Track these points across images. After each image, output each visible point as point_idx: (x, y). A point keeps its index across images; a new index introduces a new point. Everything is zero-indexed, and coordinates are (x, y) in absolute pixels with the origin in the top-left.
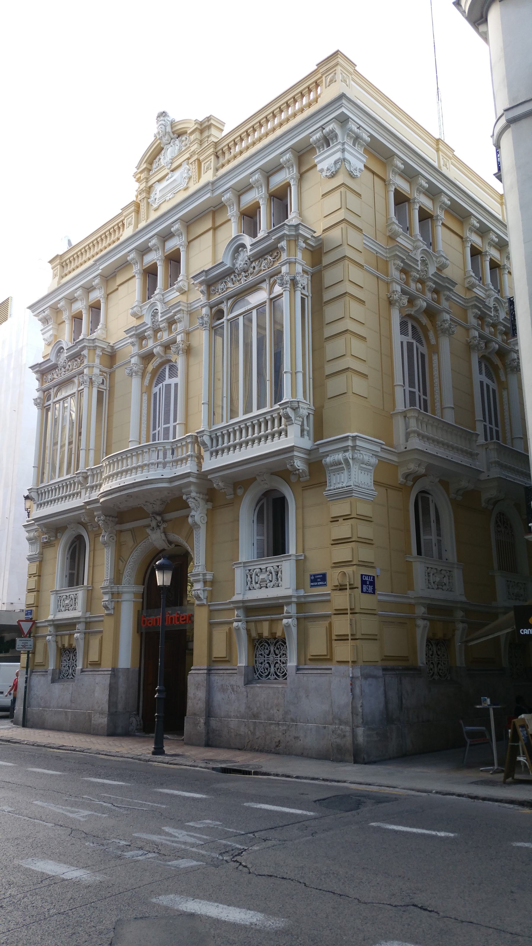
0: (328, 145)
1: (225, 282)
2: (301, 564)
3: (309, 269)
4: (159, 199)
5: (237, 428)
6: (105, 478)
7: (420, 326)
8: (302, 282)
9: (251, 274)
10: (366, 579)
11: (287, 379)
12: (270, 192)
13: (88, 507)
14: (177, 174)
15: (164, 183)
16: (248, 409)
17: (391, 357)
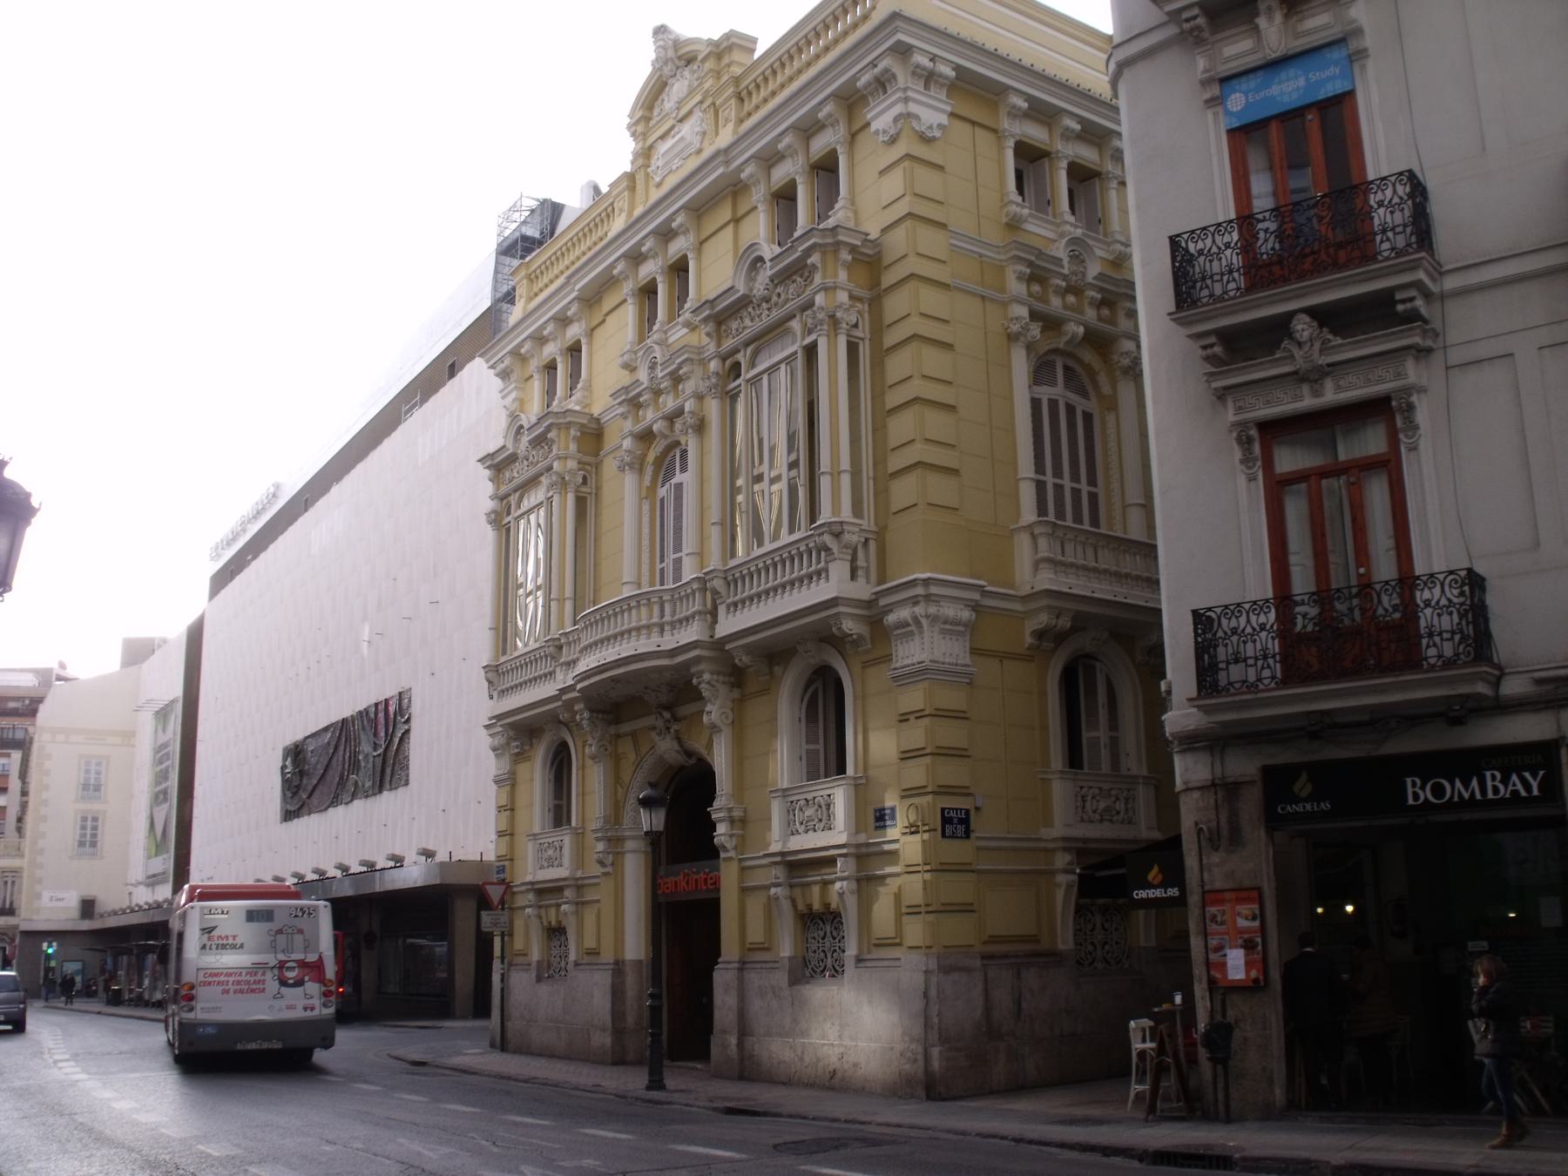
6: (585, 648)
11: (825, 484)
15: (670, 142)
16: (776, 537)
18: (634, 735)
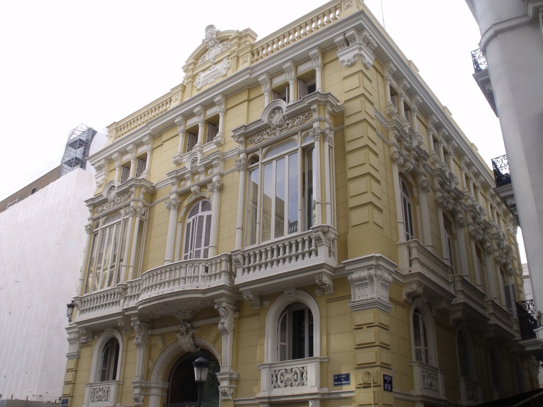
0: (348, 45)
1: (261, 135)
2: (324, 364)
3: (333, 127)
4: (202, 83)
5: (269, 248)
6: (145, 289)
7: (409, 181)
8: (329, 135)
9: (285, 129)
10: (387, 378)
12: (298, 75)
13: (126, 314)
14: (218, 66)
15: (208, 72)
17: (394, 200)
18: (162, 335)
